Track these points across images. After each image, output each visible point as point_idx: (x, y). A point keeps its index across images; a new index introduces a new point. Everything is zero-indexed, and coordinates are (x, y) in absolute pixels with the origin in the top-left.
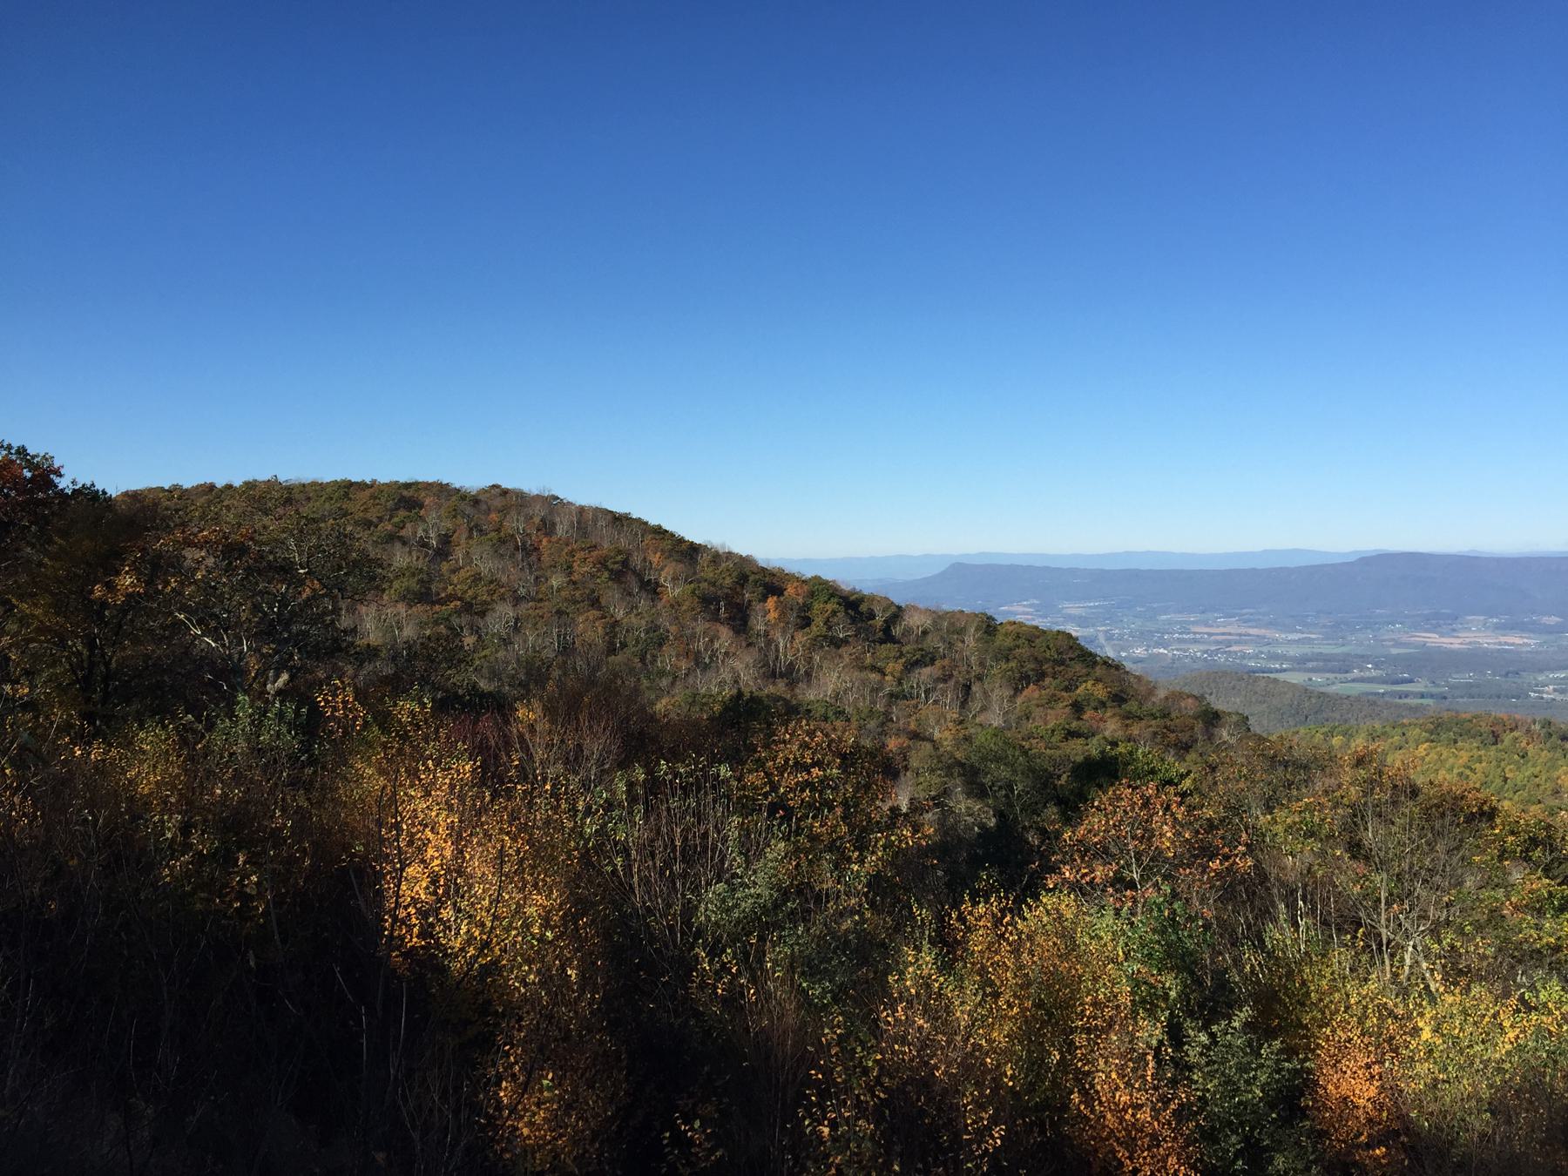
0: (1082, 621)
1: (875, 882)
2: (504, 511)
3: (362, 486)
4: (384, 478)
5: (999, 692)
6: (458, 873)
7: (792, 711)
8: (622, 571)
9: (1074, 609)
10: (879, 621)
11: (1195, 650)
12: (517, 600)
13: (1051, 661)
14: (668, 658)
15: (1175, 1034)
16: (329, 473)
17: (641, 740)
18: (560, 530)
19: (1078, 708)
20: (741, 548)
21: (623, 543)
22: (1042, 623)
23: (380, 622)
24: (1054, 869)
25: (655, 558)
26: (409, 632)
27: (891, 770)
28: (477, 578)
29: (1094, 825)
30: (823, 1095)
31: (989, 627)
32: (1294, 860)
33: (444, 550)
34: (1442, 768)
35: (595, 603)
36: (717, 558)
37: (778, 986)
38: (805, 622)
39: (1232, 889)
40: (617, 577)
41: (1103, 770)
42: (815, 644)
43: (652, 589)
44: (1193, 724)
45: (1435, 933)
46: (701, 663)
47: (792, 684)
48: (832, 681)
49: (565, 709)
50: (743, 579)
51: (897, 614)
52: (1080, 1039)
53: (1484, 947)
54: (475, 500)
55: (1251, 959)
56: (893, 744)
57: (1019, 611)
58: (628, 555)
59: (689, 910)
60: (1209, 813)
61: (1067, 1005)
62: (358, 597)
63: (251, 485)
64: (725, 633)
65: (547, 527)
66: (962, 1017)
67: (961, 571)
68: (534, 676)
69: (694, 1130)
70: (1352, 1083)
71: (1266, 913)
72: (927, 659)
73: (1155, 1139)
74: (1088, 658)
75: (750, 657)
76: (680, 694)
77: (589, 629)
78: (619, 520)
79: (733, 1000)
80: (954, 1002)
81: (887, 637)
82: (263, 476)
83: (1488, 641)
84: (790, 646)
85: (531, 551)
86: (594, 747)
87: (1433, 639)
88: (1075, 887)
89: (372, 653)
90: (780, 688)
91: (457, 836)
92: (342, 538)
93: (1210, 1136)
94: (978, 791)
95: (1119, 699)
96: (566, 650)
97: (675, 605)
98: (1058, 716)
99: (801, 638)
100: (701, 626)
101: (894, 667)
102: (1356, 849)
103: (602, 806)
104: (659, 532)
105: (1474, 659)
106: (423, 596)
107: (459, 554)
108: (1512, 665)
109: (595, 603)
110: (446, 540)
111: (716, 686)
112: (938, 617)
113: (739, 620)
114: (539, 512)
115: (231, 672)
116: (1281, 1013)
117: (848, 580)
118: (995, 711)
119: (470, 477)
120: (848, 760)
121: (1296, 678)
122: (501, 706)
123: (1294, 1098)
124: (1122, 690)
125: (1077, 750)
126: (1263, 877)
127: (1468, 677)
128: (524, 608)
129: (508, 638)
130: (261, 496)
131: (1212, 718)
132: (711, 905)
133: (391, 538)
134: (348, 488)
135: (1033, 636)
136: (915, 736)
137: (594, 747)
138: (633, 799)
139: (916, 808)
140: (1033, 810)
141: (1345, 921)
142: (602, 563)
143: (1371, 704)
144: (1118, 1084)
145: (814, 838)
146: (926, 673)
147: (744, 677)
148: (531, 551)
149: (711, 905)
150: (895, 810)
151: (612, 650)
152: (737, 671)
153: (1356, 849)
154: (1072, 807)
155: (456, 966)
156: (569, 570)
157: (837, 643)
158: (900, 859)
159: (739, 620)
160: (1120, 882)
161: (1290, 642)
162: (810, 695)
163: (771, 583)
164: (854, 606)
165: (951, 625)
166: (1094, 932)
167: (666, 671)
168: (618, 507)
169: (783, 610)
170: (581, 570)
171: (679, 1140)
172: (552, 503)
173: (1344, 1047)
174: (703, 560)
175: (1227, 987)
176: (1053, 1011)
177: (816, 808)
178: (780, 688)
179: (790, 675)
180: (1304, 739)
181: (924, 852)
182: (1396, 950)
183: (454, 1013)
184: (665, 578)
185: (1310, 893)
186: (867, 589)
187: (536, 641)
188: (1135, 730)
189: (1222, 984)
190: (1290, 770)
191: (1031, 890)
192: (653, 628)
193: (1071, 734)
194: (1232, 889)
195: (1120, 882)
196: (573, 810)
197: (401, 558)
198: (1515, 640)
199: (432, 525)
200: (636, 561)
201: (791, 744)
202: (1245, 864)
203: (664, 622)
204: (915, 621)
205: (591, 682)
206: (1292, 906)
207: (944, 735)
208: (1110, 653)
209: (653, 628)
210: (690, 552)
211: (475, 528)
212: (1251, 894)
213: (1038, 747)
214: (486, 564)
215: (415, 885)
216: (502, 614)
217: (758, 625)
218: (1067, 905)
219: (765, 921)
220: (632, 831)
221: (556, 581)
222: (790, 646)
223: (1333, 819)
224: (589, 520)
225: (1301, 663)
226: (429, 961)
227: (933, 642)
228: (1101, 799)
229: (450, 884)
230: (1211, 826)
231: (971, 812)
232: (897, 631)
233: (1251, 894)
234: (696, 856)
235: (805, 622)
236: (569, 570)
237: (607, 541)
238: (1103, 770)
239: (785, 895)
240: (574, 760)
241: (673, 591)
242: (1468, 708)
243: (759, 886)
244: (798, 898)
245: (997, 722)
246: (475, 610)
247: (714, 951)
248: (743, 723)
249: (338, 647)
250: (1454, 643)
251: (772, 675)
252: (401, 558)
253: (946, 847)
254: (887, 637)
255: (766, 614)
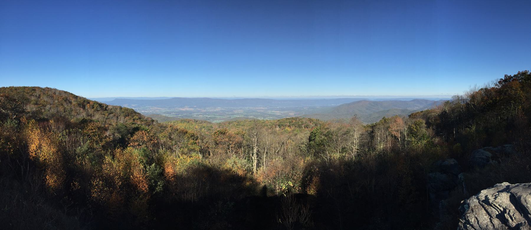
0: (135, 107)
1: (103, 146)
2: (48, 91)
3: (27, 87)
4: (30, 86)
5: (122, 118)
6: (41, 146)
7: (91, 121)
8: (66, 100)
9: (133, 105)
10: (104, 107)
11: (151, 111)
12: (50, 104)
13: (130, 113)
14: (73, 113)
15: (145, 167)
16: (22, 85)
17: (68, 126)
18: (57, 94)
19: (134, 120)
20: (84, 97)
21: (66, 96)
22: (129, 108)
23: (30, 108)
24: (129, 144)
25: (71, 98)
26: (34, 109)
27: (106, 130)
28: (44, 101)
29: (135, 137)
30: (95, 178)
31: (121, 108)
32: (162, 140)
33: (39, 97)
34: (181, 126)
35: (62, 105)
36: (80, 98)
37: (87, 163)
38: (93, 108)
39: (154, 145)
40: (65, 101)
41: (137, 129)
42: (94, 111)
43: (71, 103)
44: (150, 122)
45: (180, 148)
46: (78, 114)
47: (91, 117)
48: (97, 116)
49: (57, 121)
50: (84, 101)
51: (107, 106)
52: (132, 168)
53: (186, 150)
54: (44, 89)
55: (157, 154)
56: (106, 126)
57: (125, 106)
58: (67, 98)
59: (75, 150)
60: (151, 135)
61: (130, 163)
62: (26, 104)
63: (10, 87)
64: (82, 110)
65: (55, 93)
66: (115, 165)
67: (117, 100)
68: (53, 115)
69: (76, 183)
70: (169, 170)
71: (159, 148)
72: (112, 113)
73: (142, 182)
74: (135, 113)
75: (85, 113)
76: (75, 119)
77: (61, 109)
78: (66, 92)
79: (81, 164)
80: (112, 165)
81: (106, 110)
82: (12, 86)
83: (188, 109)
84: (91, 111)
85: (52, 97)
86: (61, 127)
87: (181, 109)
88: (132, 146)
89: (29, 112)
90: (89, 118)
91: (39, 139)
92: (23, 95)
93: (150, 180)
94: (119, 132)
95: (140, 118)
96: (58, 112)
97: (74, 105)
98: (131, 121)
99: (93, 110)
100: (78, 108)
101: (107, 114)
102: (170, 138)
103: (60, 135)
104: (72, 94)
105: (186, 112)
106: (36, 104)
107: (41, 98)
108: (191, 112)
109: (62, 105)
110: (40, 95)
111: (80, 117)
112: (113, 107)
113: (84, 107)
114: (53, 91)
115: (7, 115)
116: (160, 162)
117: (100, 101)
118: (122, 120)
119: (43, 86)
120: (99, 128)
121: (164, 115)
122: (47, 120)
123: (162, 174)
124: (140, 117)
125: (134, 126)
126: (158, 143)
127: (185, 114)
128: (51, 106)
129: (49, 110)
130: (11, 89)
131: (153, 121)
132: (78, 150)
133: (31, 95)
134: (25, 88)
135: (127, 109)
136: (110, 124)
137: (61, 127)
138: (66, 134)
139: (110, 135)
140: (126, 135)
141: (170, 148)
142: (63, 99)
143: (174, 118)
144: (137, 174)
145: (94, 140)
146: (112, 115)
147: (85, 116)
148: (52, 97)
149: (78, 150)
150: (106, 136)
151: (65, 112)
152: (83, 115)
153: (170, 138)
154: (132, 134)
155: (41, 159)
156: (58, 100)
157: (98, 111)
158: (107, 143)
159: (84, 107)
160: (139, 145)
161: (163, 110)
162: (94, 119)
163: (88, 102)
164: (101, 105)
165: (115, 108)
166: (135, 153)
167: (73, 116)
168: (65, 90)
169: (90, 105)
170: (60, 100)
171: (74, 185)
172: (55, 90)
173: (168, 165)
174: (78, 98)
175: (153, 159)
176: (128, 165)
177: (94, 136)
178: (89, 118)
179: (91, 116)
180: (164, 123)
181: (111, 142)
182: (175, 151)
183: (38, 167)
184: (73, 101)
185: (164, 145)
186: (102, 103)
187: (53, 111)
188: (143, 123)
189: (153, 158)
190: (163, 128)
191: (127, 146)
192: (71, 109)
193: (133, 124)
194: (154, 145)
195: (139, 145)
196: (58, 136)
197: (33, 98)
198: (191, 109)
199: (38, 93)
200: (68, 98)
201: (90, 126)
202: (156, 142)
203: (73, 108)
204: (110, 107)
205: (61, 116)
206: (162, 147)
207: (114, 124)
208: (139, 112)
209: (71, 109)
210: (76, 97)
211: (44, 94)
212: (156, 145)
213: (128, 126)
214: (46, 99)
215: (33, 147)
216: (48, 107)
217: (86, 108)
218: (131, 148)
219: (87, 152)
220: (67, 139)
221: (56, 101)
222: (91, 111)
223: (167, 134)
224: (61, 92)
225: (165, 113)
226: (37, 158)
227: (113, 110)
228: (137, 133)
229: (40, 147)
230: (152, 136)
231: (118, 136)
232: (107, 109)
233: (156, 145)
234: (76, 143)
235: (93, 108)
236: (58, 100)
237: (64, 96)
238: (137, 129)
239: (89, 149)
240: (58, 128)
241: (74, 103)
242: (185, 118)
243: (85, 147)
244: (91, 149)
245: (122, 122)
246: (44, 106)
247: (78, 157)
248: (84, 122)
249: (23, 111)
250: (184, 110)
251: (88, 116)
252: (33, 98)
253: (114, 141)
254: (106, 110)
255: (88, 106)
